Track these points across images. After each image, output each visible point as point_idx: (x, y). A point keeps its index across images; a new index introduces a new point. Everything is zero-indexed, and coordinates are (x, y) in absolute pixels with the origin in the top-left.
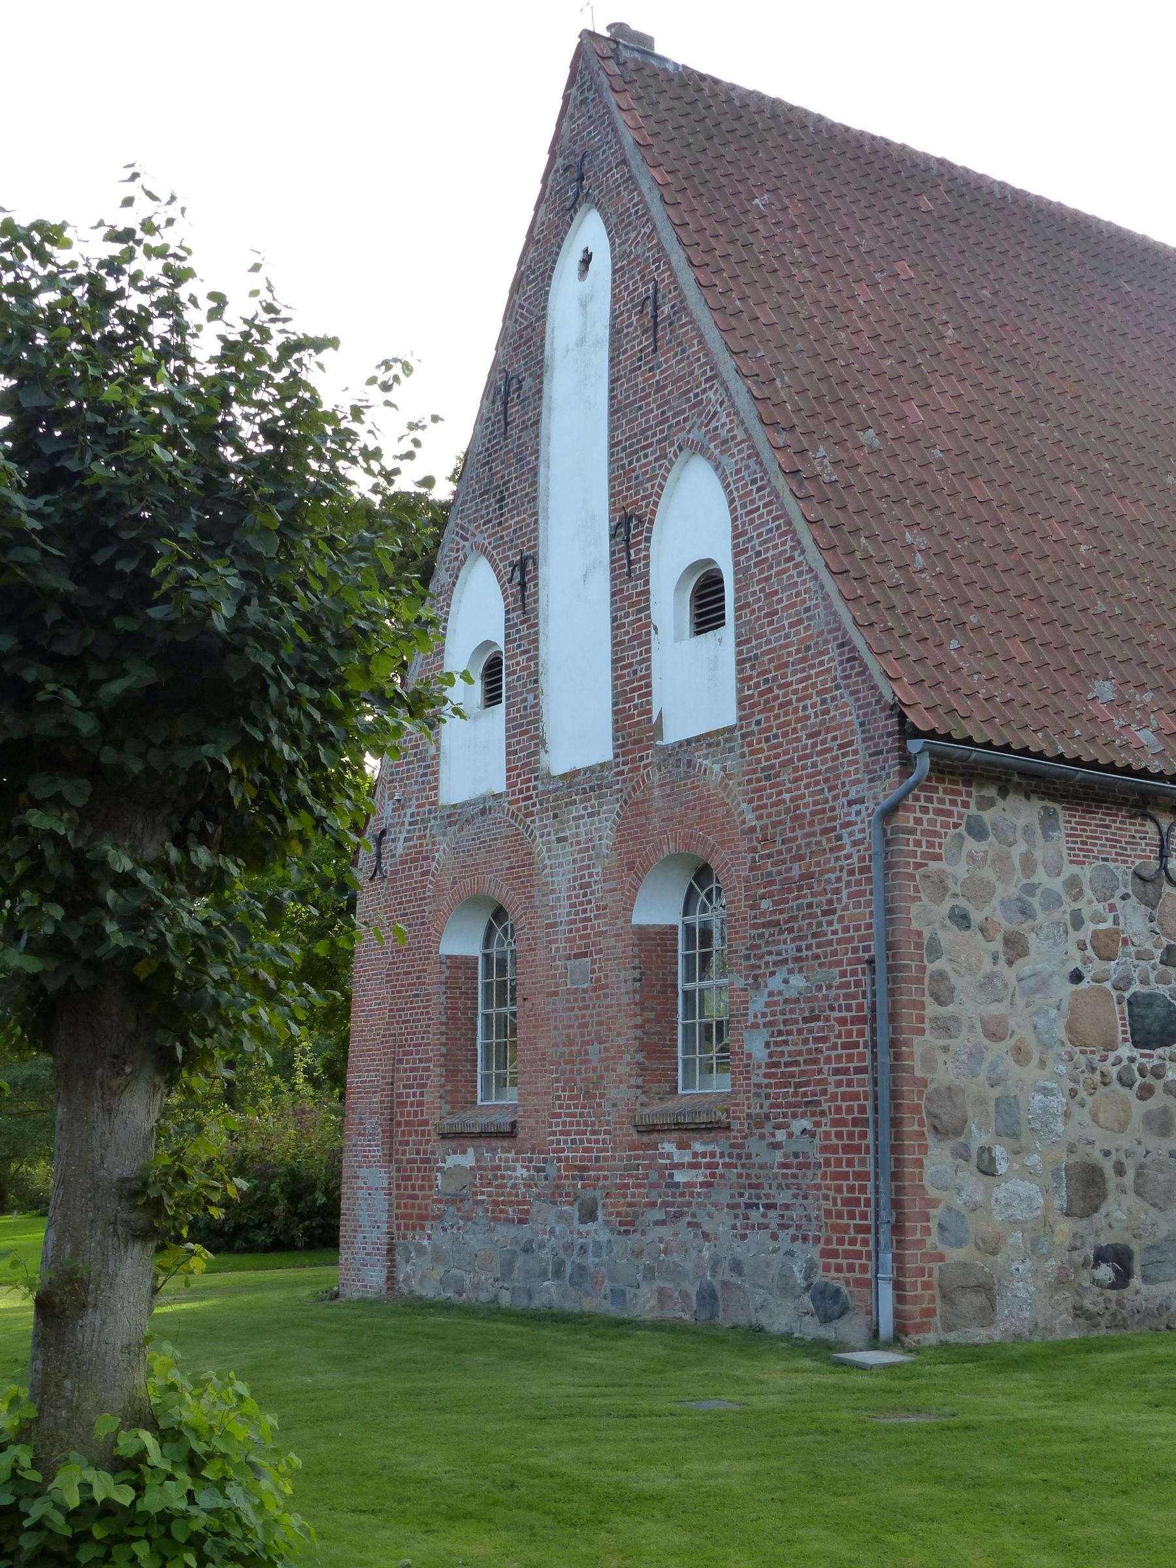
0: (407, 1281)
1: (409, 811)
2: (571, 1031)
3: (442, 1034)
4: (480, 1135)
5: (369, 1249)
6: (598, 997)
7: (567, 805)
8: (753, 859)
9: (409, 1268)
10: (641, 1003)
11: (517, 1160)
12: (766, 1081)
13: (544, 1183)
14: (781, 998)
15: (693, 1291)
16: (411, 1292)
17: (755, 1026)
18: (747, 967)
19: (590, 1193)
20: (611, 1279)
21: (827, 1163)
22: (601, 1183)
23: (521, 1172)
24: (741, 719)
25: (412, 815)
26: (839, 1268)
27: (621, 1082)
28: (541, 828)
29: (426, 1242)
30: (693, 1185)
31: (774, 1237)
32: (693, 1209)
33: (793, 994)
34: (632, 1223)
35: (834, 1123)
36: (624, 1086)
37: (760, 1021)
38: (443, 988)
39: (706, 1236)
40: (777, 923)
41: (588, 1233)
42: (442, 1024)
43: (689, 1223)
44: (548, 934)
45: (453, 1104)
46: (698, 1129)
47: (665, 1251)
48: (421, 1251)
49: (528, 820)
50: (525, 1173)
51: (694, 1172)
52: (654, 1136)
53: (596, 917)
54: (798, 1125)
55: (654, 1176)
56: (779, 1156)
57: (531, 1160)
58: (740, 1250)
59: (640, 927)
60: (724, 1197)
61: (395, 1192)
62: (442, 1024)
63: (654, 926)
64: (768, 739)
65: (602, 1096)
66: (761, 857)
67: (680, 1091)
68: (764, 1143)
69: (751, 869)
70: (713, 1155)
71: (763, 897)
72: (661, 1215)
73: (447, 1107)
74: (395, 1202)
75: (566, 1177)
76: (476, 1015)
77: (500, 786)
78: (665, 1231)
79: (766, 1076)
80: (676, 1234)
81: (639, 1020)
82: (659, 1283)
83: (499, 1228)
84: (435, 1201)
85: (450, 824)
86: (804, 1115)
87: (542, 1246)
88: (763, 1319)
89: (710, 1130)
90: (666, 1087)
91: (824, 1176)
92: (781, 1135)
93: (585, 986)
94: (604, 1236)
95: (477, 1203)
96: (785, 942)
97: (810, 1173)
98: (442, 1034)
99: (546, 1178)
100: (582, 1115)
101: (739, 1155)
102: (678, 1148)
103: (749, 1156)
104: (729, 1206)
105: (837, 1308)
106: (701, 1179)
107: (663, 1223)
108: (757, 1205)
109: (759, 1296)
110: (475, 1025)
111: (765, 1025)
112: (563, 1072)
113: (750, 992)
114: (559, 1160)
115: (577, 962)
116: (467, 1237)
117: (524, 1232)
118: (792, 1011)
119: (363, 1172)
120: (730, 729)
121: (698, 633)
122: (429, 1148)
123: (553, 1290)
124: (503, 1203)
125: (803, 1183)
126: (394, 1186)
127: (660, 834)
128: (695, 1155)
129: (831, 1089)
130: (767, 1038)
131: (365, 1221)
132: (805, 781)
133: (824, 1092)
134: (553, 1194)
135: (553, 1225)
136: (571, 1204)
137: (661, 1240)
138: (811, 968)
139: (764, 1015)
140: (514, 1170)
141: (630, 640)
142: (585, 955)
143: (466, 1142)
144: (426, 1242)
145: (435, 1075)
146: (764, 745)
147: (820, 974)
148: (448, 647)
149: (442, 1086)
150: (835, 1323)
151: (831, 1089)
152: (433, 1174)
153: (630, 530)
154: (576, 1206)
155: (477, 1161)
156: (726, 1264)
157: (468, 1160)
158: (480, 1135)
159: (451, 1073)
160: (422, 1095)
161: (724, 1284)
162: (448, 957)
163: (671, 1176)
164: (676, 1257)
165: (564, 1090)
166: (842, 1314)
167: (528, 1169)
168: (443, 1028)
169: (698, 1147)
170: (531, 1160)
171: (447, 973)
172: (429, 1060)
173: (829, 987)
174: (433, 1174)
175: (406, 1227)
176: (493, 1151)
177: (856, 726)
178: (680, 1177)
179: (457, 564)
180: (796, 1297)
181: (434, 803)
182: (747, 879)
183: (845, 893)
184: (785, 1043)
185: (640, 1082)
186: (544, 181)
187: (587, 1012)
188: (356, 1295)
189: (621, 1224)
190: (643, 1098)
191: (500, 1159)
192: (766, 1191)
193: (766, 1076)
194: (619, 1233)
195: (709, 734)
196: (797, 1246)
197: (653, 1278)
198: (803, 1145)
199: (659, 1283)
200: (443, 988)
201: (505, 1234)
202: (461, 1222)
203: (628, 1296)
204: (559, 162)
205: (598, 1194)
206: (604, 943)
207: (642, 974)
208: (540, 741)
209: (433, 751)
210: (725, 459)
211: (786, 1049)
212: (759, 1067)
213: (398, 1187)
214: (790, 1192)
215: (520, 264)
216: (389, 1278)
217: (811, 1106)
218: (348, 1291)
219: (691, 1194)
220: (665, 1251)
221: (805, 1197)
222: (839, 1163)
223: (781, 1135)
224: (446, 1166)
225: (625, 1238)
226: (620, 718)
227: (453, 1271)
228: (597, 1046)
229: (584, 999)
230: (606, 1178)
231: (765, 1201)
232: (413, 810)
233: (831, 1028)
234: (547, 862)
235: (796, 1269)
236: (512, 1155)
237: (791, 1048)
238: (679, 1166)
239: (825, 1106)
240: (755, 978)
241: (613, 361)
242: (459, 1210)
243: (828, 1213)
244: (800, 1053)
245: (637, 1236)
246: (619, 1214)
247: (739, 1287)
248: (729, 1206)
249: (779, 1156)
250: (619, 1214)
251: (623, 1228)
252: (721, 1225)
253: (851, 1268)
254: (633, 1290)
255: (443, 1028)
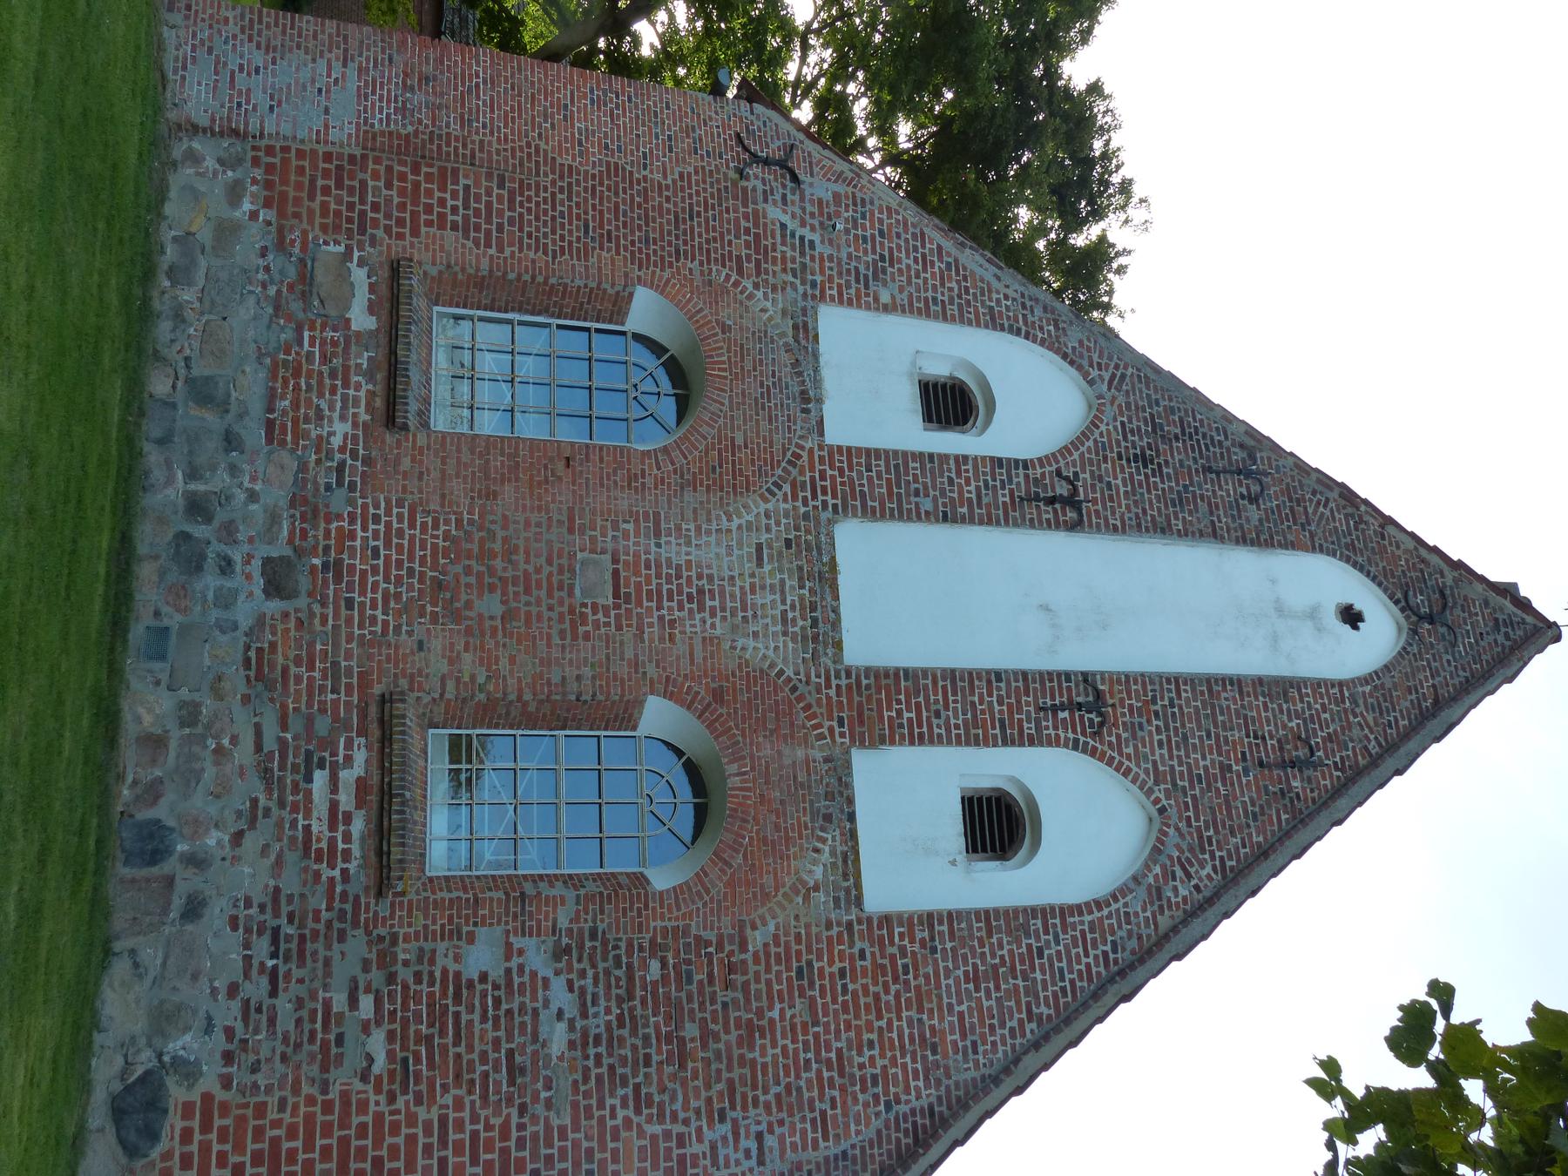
0: (193, 158)
3: (533, 278)
4: (393, 352)
7: (800, 568)
8: (708, 944)
9: (210, 163)
11: (355, 425)
12: (438, 974)
13: (322, 481)
14: (539, 1005)
15: (161, 812)
16: (174, 164)
17: (509, 952)
19: (304, 583)
20: (185, 630)
21: (328, 1107)
22: (317, 608)
23: (341, 429)
25: (812, 243)
26: (187, 1136)
27: (451, 662)
28: (776, 511)
29: (247, 206)
30: (308, 815)
32: (275, 811)
35: (379, 1117)
36: (444, 668)
37: (514, 963)
39: (237, 838)
40: (631, 997)
41: (249, 577)
43: (255, 801)
44: (646, 514)
45: (439, 279)
46: (383, 812)
47: (219, 751)
48: (234, 193)
49: (787, 488)
54: (377, 1044)
55: (322, 726)
56: (339, 1001)
58: (217, 912)
60: (290, 883)
61: (321, 149)
63: (641, 713)
66: (709, 955)
67: (431, 731)
68: (357, 971)
69: (698, 938)
70: (347, 855)
71: (664, 965)
72: (269, 744)
73: (434, 272)
74: (307, 148)
75: (327, 533)
76: (552, 316)
78: (244, 754)
79: (445, 972)
80: (242, 774)
81: (527, 697)
82: (176, 735)
83: (262, 375)
84: (305, 233)
85: (796, 327)
87: (233, 470)
88: (120, 968)
89: (380, 853)
90: (438, 719)
91: (311, 1101)
92: (366, 1004)
94: (244, 614)
95: (299, 330)
97: (316, 1068)
98: (533, 278)
99: (328, 487)
100: (411, 572)
102: (359, 779)
103: (342, 937)
105: (132, 1137)
106: (315, 829)
107: (259, 747)
108: (274, 955)
109: (151, 955)
110: (539, 314)
114: (352, 521)
115: (608, 576)
116: (252, 300)
117: (254, 434)
123: (170, 492)
124: (297, 387)
125: (302, 1056)
126: (330, 148)
128: (348, 819)
129: (422, 1113)
134: (305, 501)
135: (259, 488)
136: (291, 541)
137: (234, 740)
138: (572, 1069)
140: (343, 418)
141: (973, 703)
142: (616, 595)
143: (385, 313)
144: (247, 206)
145: (480, 259)
148: (998, 334)
149: (463, 269)
150: (111, 1130)
153: (1083, 708)
154: (288, 552)
155: (358, 334)
157: (361, 319)
158: (393, 352)
159: (480, 283)
160: (455, 227)
161: (170, 881)
162: (631, 295)
163: (321, 766)
164: (210, 773)
166: (122, 1142)
167: (342, 450)
168: (540, 279)
169: (358, 826)
171: (610, 291)
172: (501, 250)
173: (549, 1104)
174: (342, 238)
175: (270, 169)
177: (844, 1145)
179: (1085, 363)
181: (823, 298)
182: (686, 933)
183: (657, 1129)
184: (484, 1019)
186: (1435, 550)
187: (543, 593)
189: (260, 650)
190: (426, 699)
191: (358, 387)
192: (297, 973)
193: (445, 972)
194: (247, 648)
195: (857, 860)
196: (219, 1040)
197: (182, 725)
198: (353, 1061)
199: (176, 735)
201: (250, 386)
202: (272, 291)
203: (157, 666)
204: (1450, 576)
206: (628, 634)
208: (875, 513)
209: (885, 298)
210: (1142, 893)
211: (476, 1017)
212: (457, 958)
213: (328, 157)
214: (292, 1027)
215: (1366, 502)
217: (402, 1073)
219: (295, 808)
220: (219, 751)
221: (284, 1058)
222: (327, 1130)
223: (366, 1004)
224: (353, 266)
225: (240, 657)
226: (890, 681)
227: (203, 263)
229: (561, 588)
230: (324, 621)
231: (282, 971)
233: (497, 1113)
234: (736, 521)
235: (188, 1037)
236: (364, 417)
237: (477, 1026)
239: (400, 1103)
240: (567, 950)
241: (1260, 683)
242: (291, 287)
243: (261, 1110)
244: (470, 1048)
245: (242, 688)
246: (273, 645)
247: (165, 910)
248: (277, 890)
249: (339, 1001)
251: (252, 654)
252: (250, 876)
254: (165, 678)
255: (540, 279)
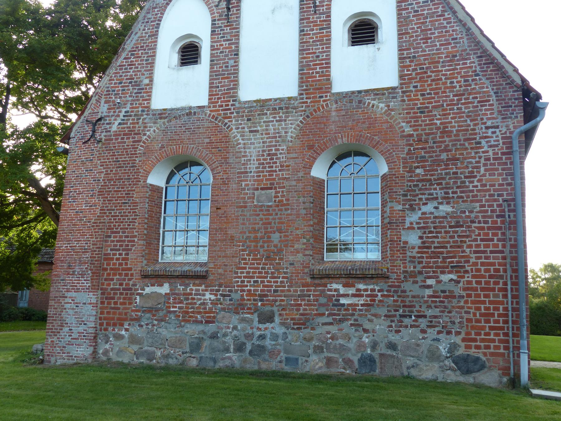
0: (106, 352)
1: (124, 110)
2: (257, 226)
5: (74, 336)
6: (281, 210)
8: (410, 150)
9: (107, 346)
10: (313, 215)
11: (206, 290)
15: (355, 359)
16: (109, 359)
17: (411, 228)
18: (403, 200)
20: (286, 351)
22: (278, 303)
24: (401, 84)
25: (126, 112)
29: (123, 332)
31: (423, 331)
33: (442, 214)
34: (304, 324)
38: (147, 200)
42: (146, 218)
44: (238, 177)
47: (332, 338)
50: (213, 297)
51: (357, 299)
52: (323, 281)
53: (280, 170)
55: (323, 300)
57: (218, 291)
59: (314, 178)
60: (383, 311)
61: (99, 305)
62: (146, 218)
64: (423, 95)
65: (280, 259)
66: (414, 149)
69: (407, 154)
73: (145, 262)
76: (161, 216)
77: (204, 102)
79: (418, 252)
80: (341, 330)
85: (161, 118)
86: (450, 272)
87: (225, 335)
93: (270, 204)
96: (435, 189)
100: (262, 268)
101: (396, 289)
103: (404, 291)
104: (385, 316)
106: (362, 302)
107: (331, 324)
108: (410, 316)
110: (160, 221)
111: (419, 228)
112: (248, 247)
113: (407, 212)
117: (211, 328)
118: (443, 222)
119: (69, 294)
120: (393, 88)
121: (352, 45)
122: (131, 283)
126: (99, 302)
127: (335, 133)
130: (420, 234)
131: (71, 319)
132: (451, 116)
133: (468, 262)
136: (252, 314)
137: (328, 333)
138: (458, 203)
139: (417, 223)
140: (204, 295)
146: (421, 98)
147: (463, 206)
151: (473, 260)
152: (134, 297)
156: (382, 345)
157: (165, 289)
158: (177, 277)
159: (149, 244)
161: (381, 355)
162: (151, 185)
164: (341, 341)
165: (248, 255)
168: (146, 221)
169: (361, 286)
170: (218, 291)
172: (135, 236)
175: (108, 324)
176: (187, 285)
178: (343, 301)
180: (441, 361)
185: (311, 253)
188: (59, 362)
189: (294, 324)
190: (313, 262)
191: (192, 290)
193: (418, 252)
195: (374, 89)
197: (323, 352)
200: (147, 200)
203: (300, 362)
205: (275, 309)
207: (313, 200)
209: (147, 81)
211: (436, 240)
213: (102, 303)
216: (94, 352)
218: (53, 359)
220: (332, 338)
223: (430, 282)
225: (296, 331)
228: (277, 235)
232: (128, 109)
235: (441, 347)
238: (344, 296)
240: (411, 205)
242: (154, 315)
245: (308, 330)
246: (292, 319)
247: (393, 356)
249: (428, 292)
250: (292, 319)
251: (295, 327)
252: (380, 326)
253: (488, 347)
